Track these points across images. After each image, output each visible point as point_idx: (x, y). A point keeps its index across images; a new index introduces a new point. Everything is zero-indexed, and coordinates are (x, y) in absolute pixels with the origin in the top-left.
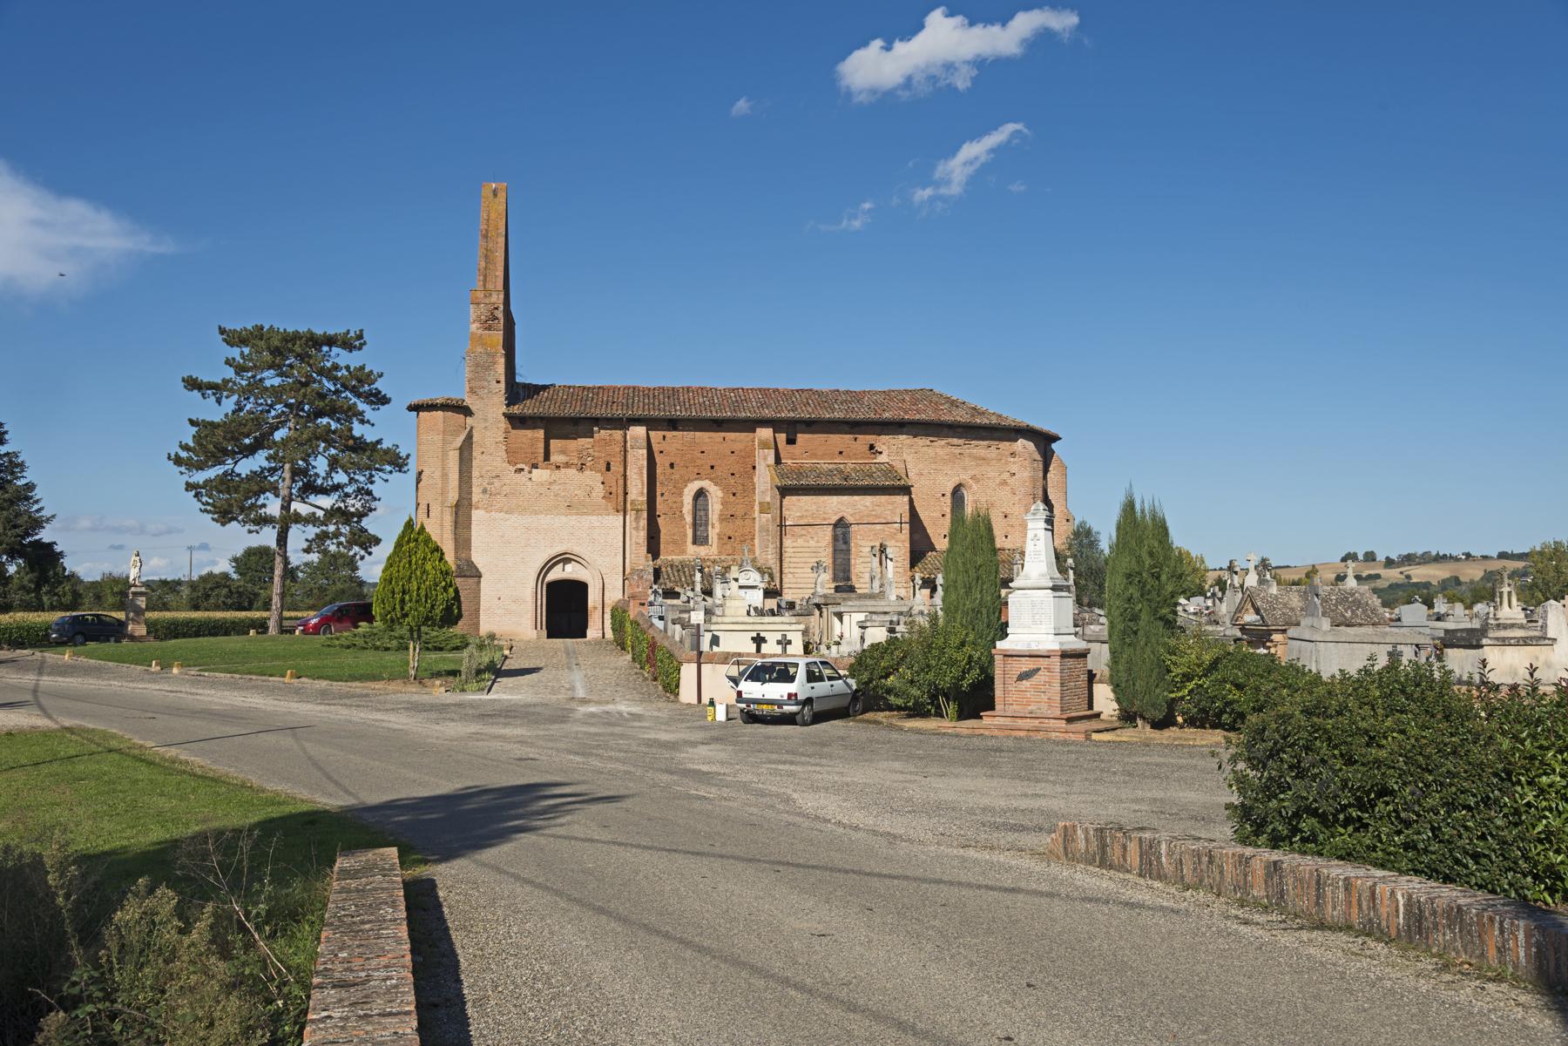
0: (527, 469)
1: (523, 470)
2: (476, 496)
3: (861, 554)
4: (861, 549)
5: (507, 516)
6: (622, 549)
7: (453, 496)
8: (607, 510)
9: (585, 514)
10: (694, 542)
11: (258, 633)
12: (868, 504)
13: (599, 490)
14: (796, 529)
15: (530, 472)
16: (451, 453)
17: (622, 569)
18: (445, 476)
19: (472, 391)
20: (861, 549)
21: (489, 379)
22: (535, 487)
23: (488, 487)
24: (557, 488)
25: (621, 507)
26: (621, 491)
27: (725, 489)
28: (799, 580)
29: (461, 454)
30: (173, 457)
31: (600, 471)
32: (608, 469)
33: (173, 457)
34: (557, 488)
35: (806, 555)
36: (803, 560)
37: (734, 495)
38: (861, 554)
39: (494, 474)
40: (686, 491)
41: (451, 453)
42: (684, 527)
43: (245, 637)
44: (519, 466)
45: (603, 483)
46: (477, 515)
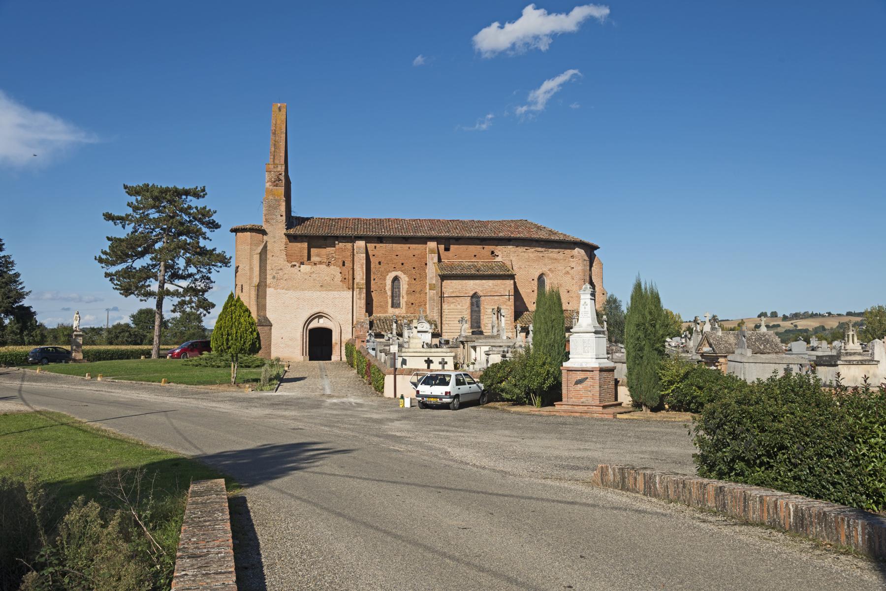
0: (298, 265)
1: (295, 265)
2: (269, 280)
3: (487, 313)
4: (487, 310)
5: (287, 292)
6: (351, 310)
7: (256, 280)
8: (343, 288)
9: (331, 290)
10: (392, 306)
11: (146, 357)
12: (490, 285)
13: (339, 277)
14: (450, 299)
15: (300, 267)
16: (255, 256)
17: (351, 321)
18: (251, 269)
19: (267, 221)
20: (487, 310)
21: (277, 214)
22: (302, 275)
23: (276, 275)
24: (315, 276)
25: (351, 287)
26: (351, 278)
27: (410, 276)
28: (451, 328)
29: (260, 257)
30: (98, 258)
31: (339, 266)
32: (344, 265)
33: (98, 258)
34: (315, 276)
35: (456, 313)
36: (454, 316)
37: (415, 279)
38: (487, 313)
39: (279, 268)
40: (388, 277)
41: (255, 256)
42: (386, 298)
43: (138, 360)
45: (341, 273)
46: (269, 291)
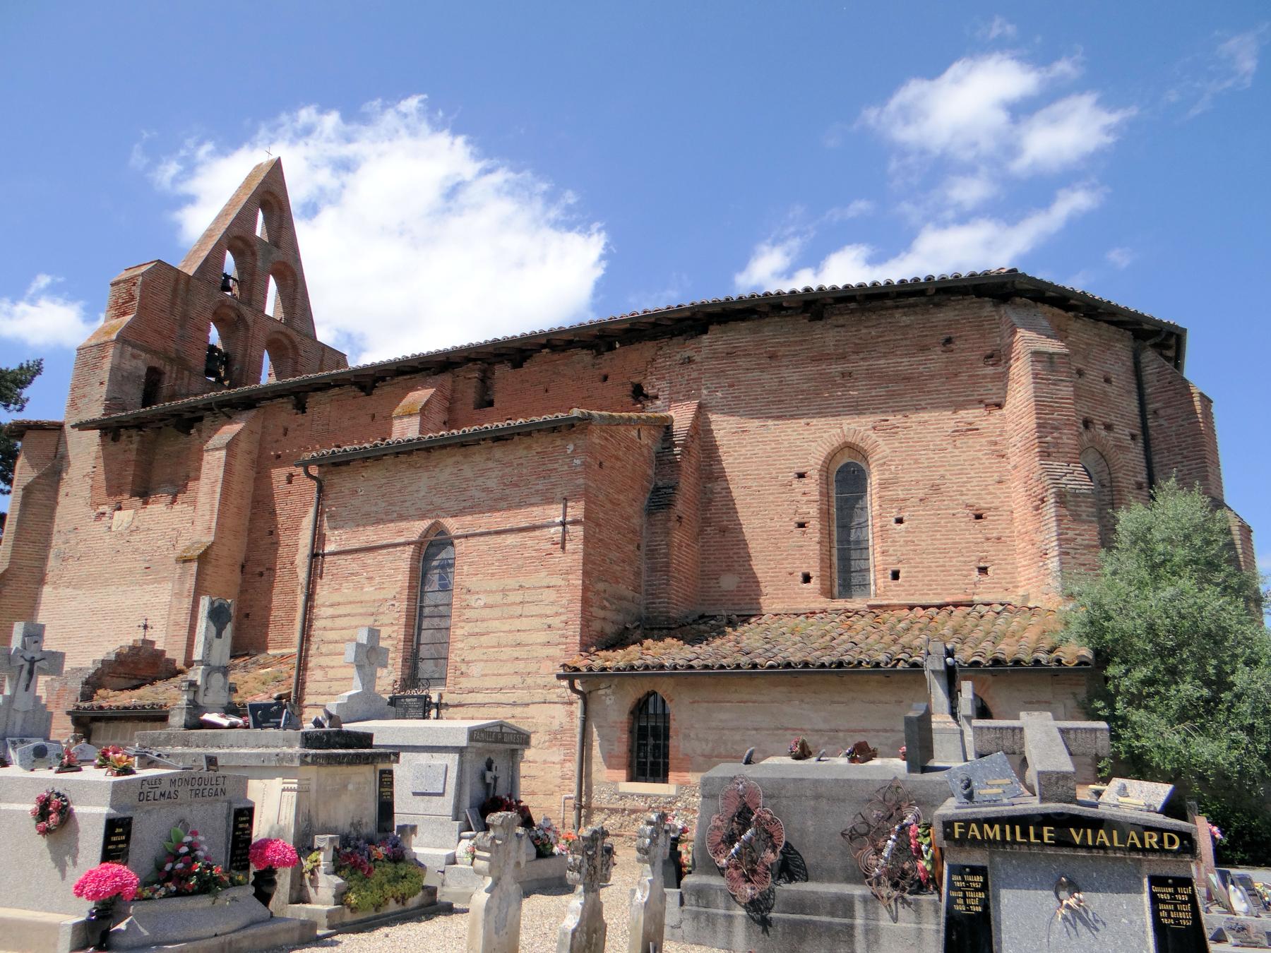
12: (492, 484)
44: (102, 509)
